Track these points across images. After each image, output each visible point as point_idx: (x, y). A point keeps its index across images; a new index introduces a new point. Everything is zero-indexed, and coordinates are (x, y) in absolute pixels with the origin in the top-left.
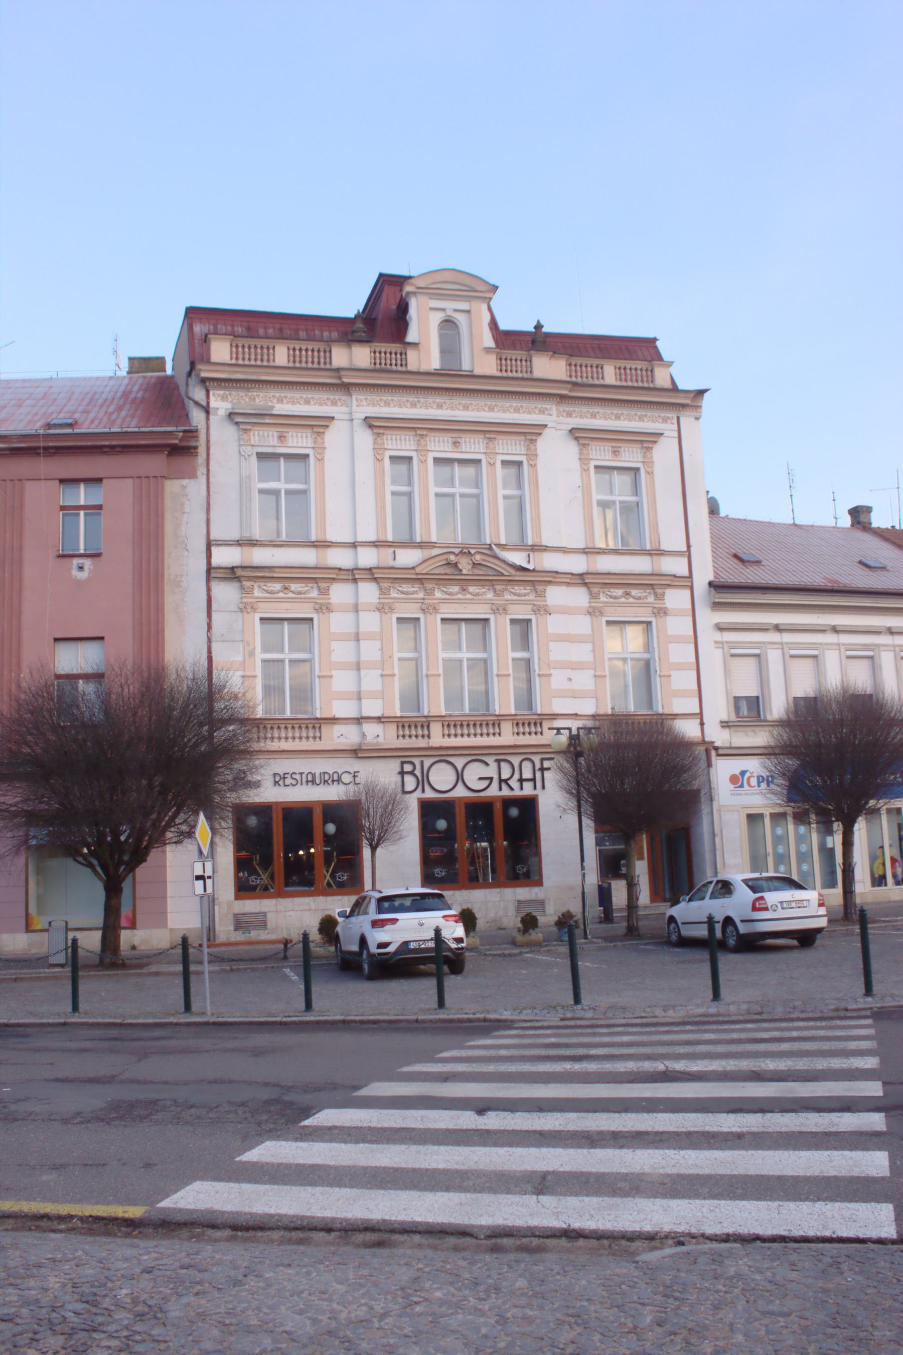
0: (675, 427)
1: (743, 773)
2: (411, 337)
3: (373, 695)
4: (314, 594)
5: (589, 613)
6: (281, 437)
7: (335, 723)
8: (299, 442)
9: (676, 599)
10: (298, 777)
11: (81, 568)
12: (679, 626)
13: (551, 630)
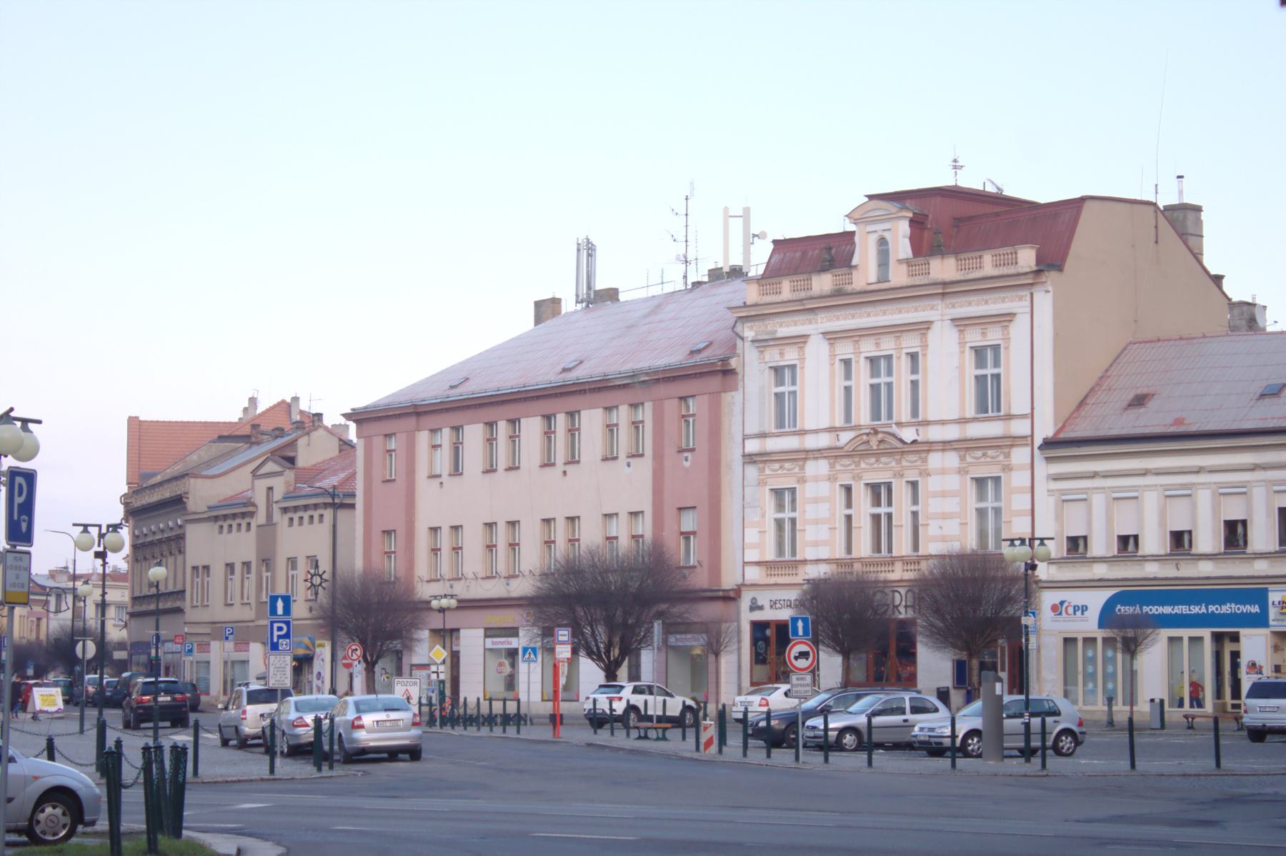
0: (1028, 303)
1: (1062, 603)
2: (854, 262)
3: (753, 546)
4: (797, 470)
5: (959, 472)
6: (781, 354)
7: (806, 564)
8: (791, 356)
9: (1020, 455)
10: (782, 602)
11: (686, 459)
12: (1020, 479)
13: (931, 488)
